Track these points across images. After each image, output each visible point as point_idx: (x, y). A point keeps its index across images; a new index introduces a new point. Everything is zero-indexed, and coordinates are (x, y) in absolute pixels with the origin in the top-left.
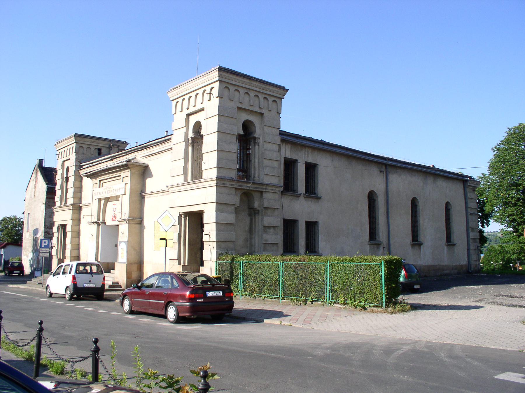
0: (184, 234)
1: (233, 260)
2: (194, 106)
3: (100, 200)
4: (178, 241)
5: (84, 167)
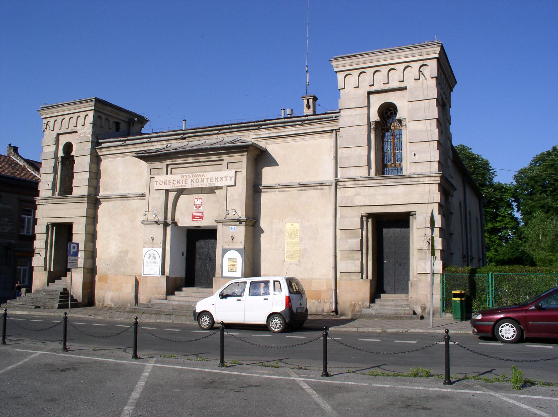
0: (51, 242)
1: (473, 272)
2: (83, 125)
3: (167, 191)
4: (45, 247)
5: (104, 145)
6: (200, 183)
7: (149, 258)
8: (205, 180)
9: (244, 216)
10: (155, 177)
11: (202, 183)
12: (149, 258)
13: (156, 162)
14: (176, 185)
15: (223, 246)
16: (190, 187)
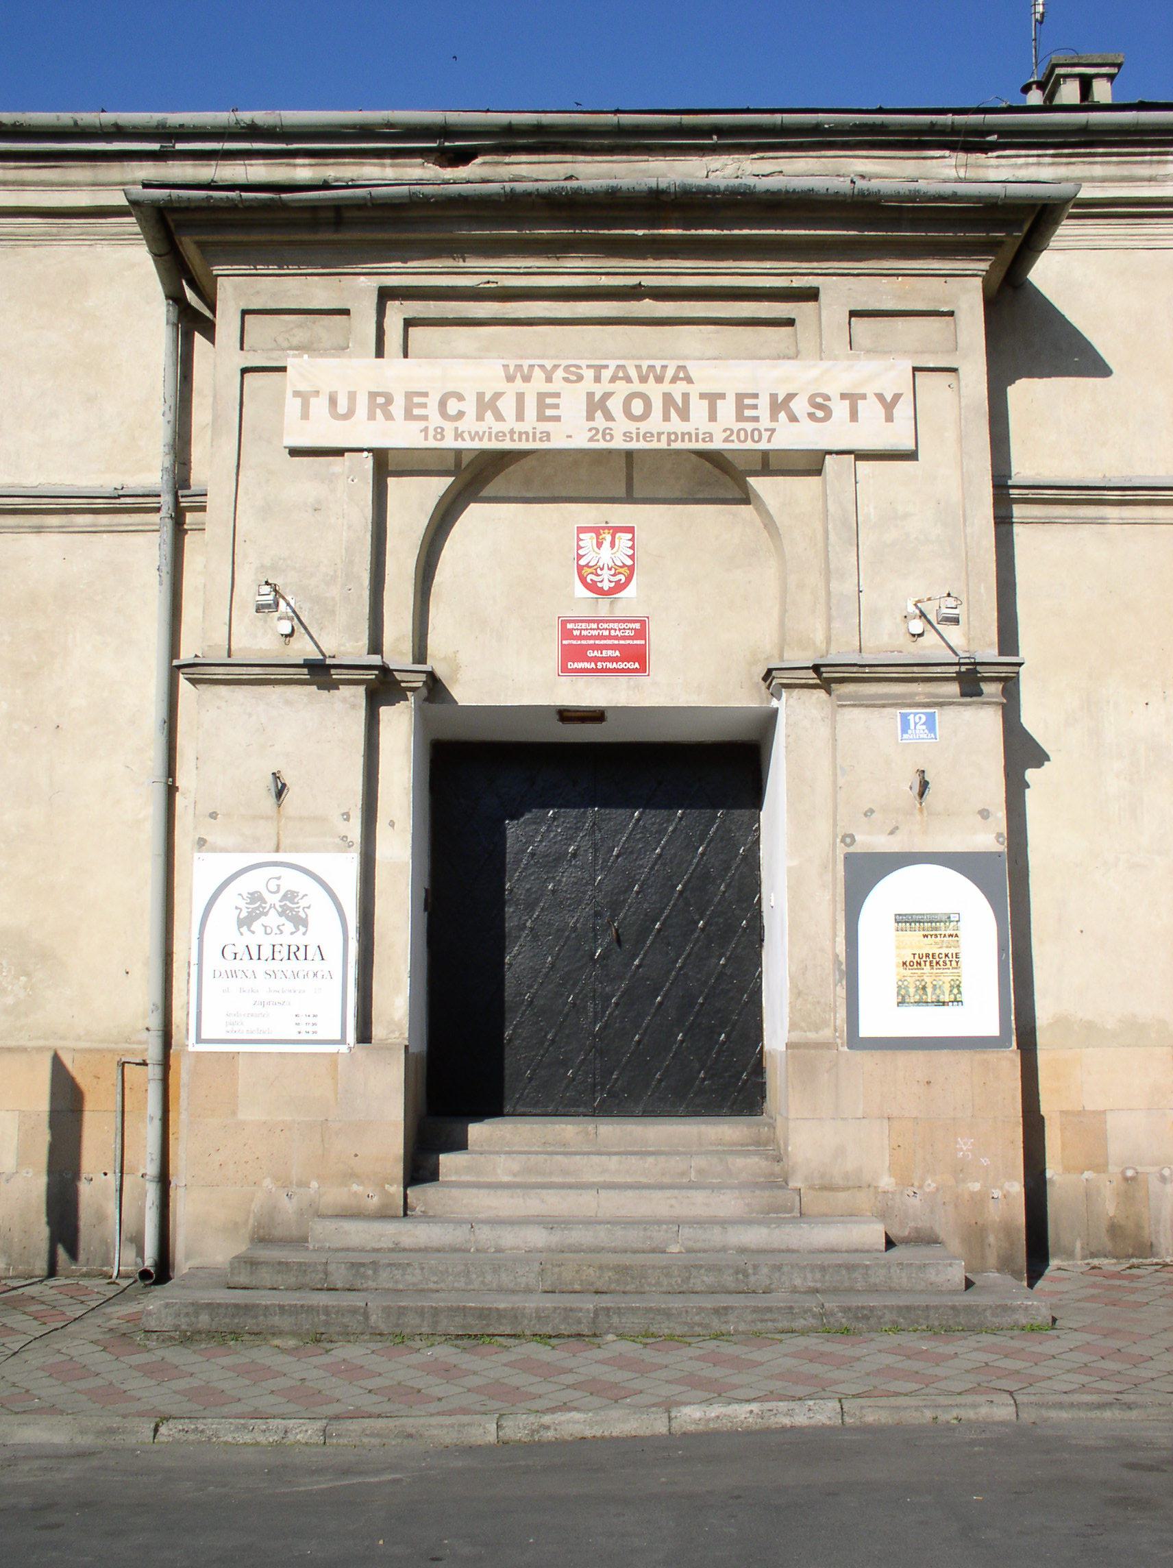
6: (655, 422)
7: (245, 922)
8: (699, 409)
9: (990, 645)
10: (291, 362)
11: (676, 425)
12: (245, 922)
13: (299, 264)
14: (469, 423)
15: (849, 839)
16: (581, 441)
